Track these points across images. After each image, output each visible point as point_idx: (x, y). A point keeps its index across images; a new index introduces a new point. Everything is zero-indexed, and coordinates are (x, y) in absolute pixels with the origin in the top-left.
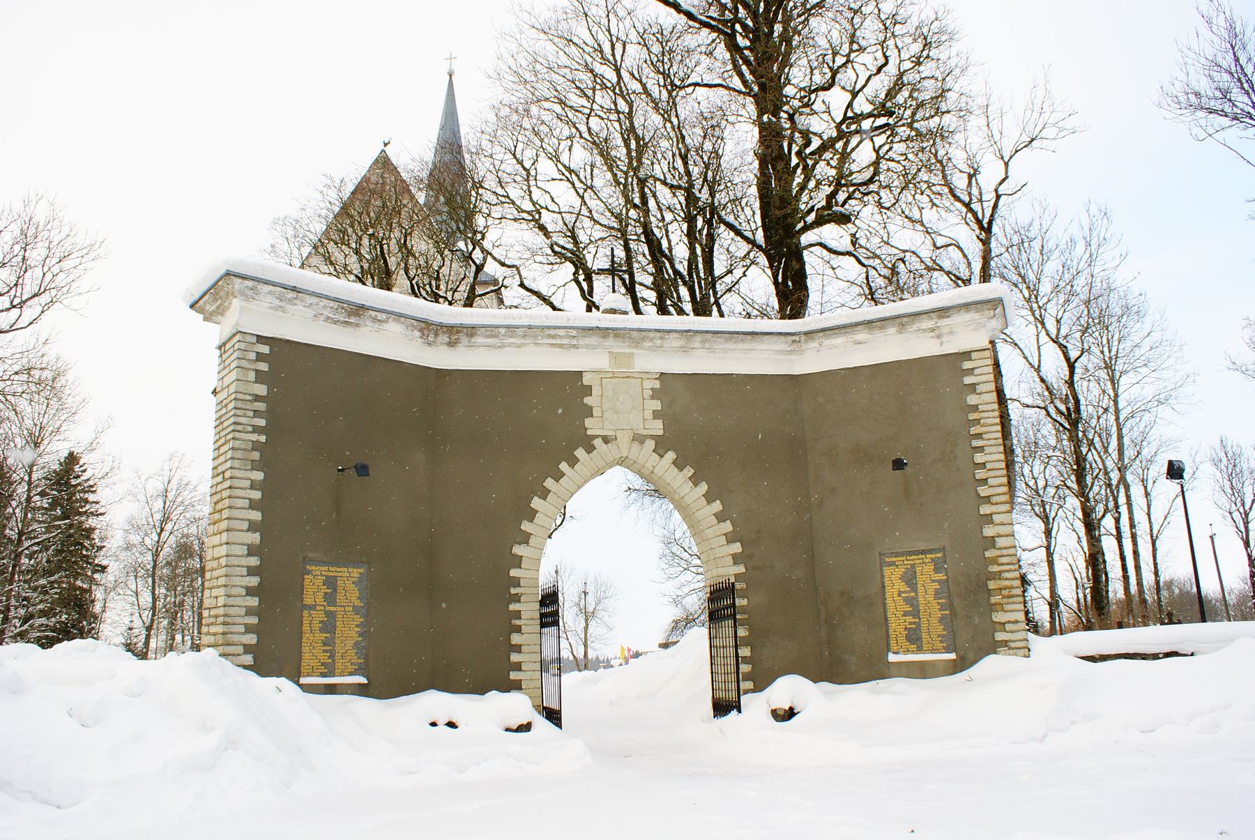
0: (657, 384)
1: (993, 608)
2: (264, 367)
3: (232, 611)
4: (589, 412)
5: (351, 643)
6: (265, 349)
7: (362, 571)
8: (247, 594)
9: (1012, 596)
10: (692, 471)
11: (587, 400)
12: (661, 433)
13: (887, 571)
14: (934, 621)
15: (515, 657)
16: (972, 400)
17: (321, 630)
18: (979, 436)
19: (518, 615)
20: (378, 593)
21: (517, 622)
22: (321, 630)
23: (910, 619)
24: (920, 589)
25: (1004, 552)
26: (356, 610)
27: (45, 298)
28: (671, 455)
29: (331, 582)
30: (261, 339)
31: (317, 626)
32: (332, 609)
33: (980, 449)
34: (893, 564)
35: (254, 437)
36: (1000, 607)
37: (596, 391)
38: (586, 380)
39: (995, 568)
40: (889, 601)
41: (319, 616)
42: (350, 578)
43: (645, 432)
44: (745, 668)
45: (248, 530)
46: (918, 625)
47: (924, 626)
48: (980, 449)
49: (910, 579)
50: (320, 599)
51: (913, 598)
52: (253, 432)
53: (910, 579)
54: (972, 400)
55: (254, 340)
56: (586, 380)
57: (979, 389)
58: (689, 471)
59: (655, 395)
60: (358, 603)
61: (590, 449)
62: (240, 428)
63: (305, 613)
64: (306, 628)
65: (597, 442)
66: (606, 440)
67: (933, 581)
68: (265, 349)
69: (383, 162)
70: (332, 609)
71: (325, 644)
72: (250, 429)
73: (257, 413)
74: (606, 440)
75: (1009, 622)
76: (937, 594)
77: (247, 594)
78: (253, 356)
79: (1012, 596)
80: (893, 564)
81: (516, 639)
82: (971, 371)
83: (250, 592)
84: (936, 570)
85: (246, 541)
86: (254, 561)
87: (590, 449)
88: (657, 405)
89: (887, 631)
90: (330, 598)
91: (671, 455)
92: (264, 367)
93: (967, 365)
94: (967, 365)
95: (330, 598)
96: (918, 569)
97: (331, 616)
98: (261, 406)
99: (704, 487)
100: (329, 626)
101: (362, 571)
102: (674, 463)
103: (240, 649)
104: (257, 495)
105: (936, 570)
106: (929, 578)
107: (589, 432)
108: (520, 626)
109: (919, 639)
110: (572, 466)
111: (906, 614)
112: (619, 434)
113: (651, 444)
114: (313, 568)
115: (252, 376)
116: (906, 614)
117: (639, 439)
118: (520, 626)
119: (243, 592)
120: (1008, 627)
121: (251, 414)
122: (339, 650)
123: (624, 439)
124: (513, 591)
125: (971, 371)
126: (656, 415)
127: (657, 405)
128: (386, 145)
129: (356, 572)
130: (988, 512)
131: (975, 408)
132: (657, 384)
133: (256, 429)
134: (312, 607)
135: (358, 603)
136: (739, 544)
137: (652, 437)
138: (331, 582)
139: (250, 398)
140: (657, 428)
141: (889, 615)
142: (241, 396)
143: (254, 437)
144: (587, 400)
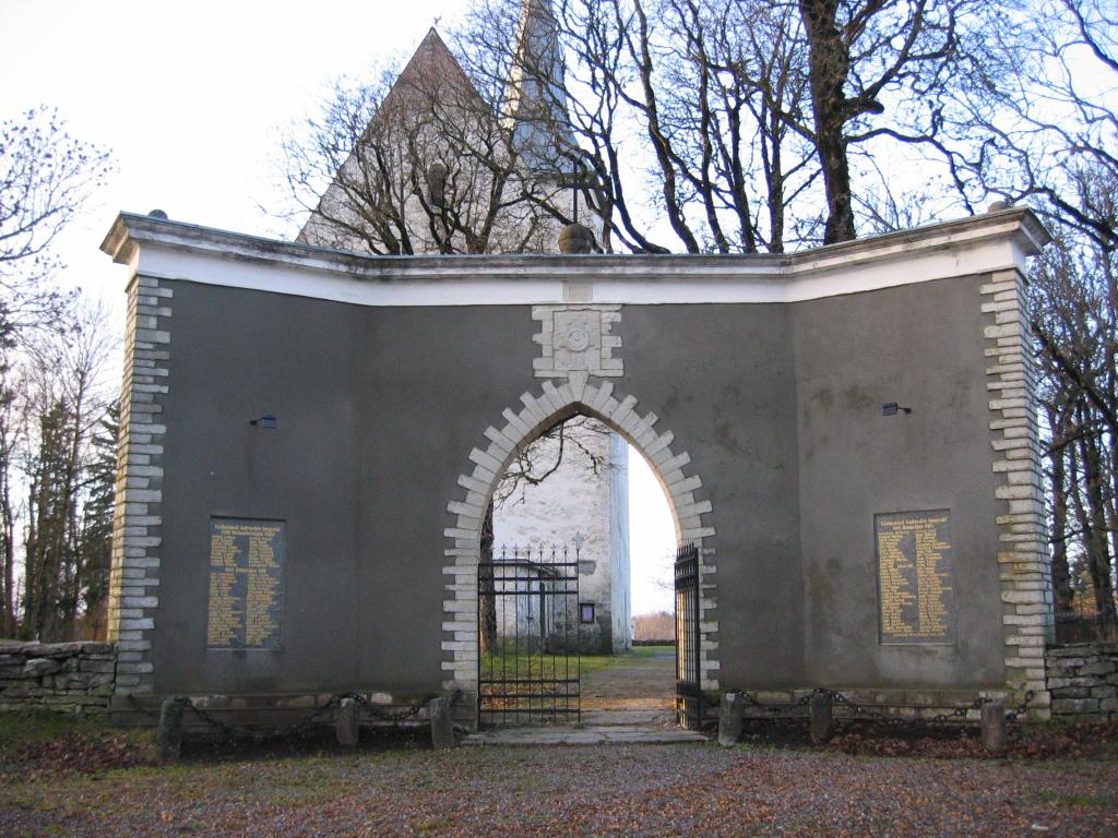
0: (618, 318)
1: (1004, 585)
2: (167, 312)
3: (131, 573)
4: (537, 350)
5: (263, 608)
6: (168, 293)
7: (278, 530)
8: (148, 555)
9: (1027, 572)
10: (655, 418)
11: (537, 338)
12: (620, 373)
13: (883, 538)
14: (934, 598)
15: (447, 626)
16: (991, 332)
17: (230, 593)
18: (996, 376)
19: (452, 579)
20: (294, 555)
21: (451, 587)
22: (230, 593)
23: (906, 595)
24: (920, 561)
25: (1020, 518)
26: (270, 571)
27: (55, 219)
28: (630, 400)
29: (242, 543)
30: (164, 282)
31: (226, 588)
32: (243, 571)
33: (997, 393)
34: (890, 529)
35: (155, 388)
36: (1009, 584)
37: (547, 327)
38: (537, 314)
39: (1008, 538)
40: (883, 574)
41: (228, 578)
42: (263, 538)
43: (602, 374)
44: (706, 645)
45: (149, 488)
46: (916, 602)
47: (922, 605)
48: (997, 393)
49: (909, 548)
50: (229, 560)
51: (911, 570)
52: (155, 383)
53: (909, 548)
54: (991, 332)
55: (155, 283)
56: (537, 314)
57: (1000, 318)
58: (652, 418)
59: (615, 329)
60: (273, 565)
61: (538, 392)
62: (140, 379)
63: (213, 576)
64: (213, 590)
65: (547, 386)
66: (557, 382)
67: (935, 551)
68: (168, 293)
69: (433, 42)
70: (243, 571)
71: (235, 608)
72: (151, 380)
73: (159, 363)
74: (557, 382)
75: (1022, 604)
76: (939, 567)
77: (148, 555)
78: (154, 301)
79: (1027, 572)
80: (890, 529)
81: (449, 606)
82: (990, 297)
83: (150, 552)
84: (939, 538)
85: (146, 500)
86: (155, 521)
87: (538, 392)
88: (617, 342)
89: (879, 609)
90: (242, 559)
91: (630, 400)
92: (167, 312)
93: (987, 289)
94: (987, 289)
95: (242, 559)
96: (918, 536)
97: (242, 578)
98: (164, 355)
99: (668, 437)
100: (239, 589)
101: (278, 530)
102: (634, 408)
103: (139, 613)
104: (158, 450)
105: (939, 538)
106: (930, 544)
107: (538, 374)
108: (454, 592)
109: (916, 618)
110: (517, 412)
111: (901, 589)
112: (572, 376)
113: (608, 387)
114: (223, 527)
115: (153, 322)
116: (901, 589)
117: (594, 381)
118: (454, 592)
119: (142, 553)
120: (1020, 609)
121: (152, 364)
122: (250, 613)
123: (577, 381)
124: (447, 553)
125: (990, 297)
126: (615, 352)
127: (617, 342)
128: (436, 21)
129: (271, 531)
130: (1003, 469)
131: (993, 342)
132: (618, 318)
133: (158, 380)
134: (221, 569)
135: (273, 565)
136: (708, 503)
137: (610, 378)
138: (242, 543)
139: (150, 346)
140: (616, 368)
141: (883, 589)
142: (141, 345)
143: (155, 388)
144: (537, 338)
